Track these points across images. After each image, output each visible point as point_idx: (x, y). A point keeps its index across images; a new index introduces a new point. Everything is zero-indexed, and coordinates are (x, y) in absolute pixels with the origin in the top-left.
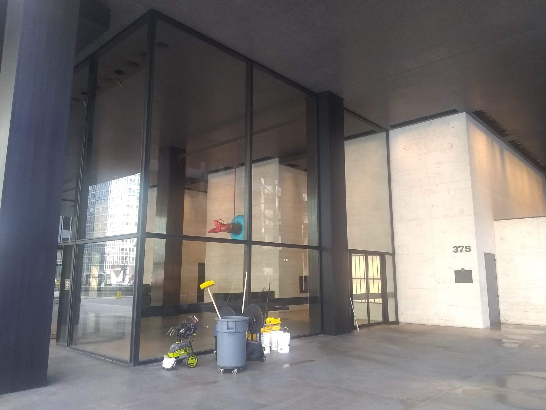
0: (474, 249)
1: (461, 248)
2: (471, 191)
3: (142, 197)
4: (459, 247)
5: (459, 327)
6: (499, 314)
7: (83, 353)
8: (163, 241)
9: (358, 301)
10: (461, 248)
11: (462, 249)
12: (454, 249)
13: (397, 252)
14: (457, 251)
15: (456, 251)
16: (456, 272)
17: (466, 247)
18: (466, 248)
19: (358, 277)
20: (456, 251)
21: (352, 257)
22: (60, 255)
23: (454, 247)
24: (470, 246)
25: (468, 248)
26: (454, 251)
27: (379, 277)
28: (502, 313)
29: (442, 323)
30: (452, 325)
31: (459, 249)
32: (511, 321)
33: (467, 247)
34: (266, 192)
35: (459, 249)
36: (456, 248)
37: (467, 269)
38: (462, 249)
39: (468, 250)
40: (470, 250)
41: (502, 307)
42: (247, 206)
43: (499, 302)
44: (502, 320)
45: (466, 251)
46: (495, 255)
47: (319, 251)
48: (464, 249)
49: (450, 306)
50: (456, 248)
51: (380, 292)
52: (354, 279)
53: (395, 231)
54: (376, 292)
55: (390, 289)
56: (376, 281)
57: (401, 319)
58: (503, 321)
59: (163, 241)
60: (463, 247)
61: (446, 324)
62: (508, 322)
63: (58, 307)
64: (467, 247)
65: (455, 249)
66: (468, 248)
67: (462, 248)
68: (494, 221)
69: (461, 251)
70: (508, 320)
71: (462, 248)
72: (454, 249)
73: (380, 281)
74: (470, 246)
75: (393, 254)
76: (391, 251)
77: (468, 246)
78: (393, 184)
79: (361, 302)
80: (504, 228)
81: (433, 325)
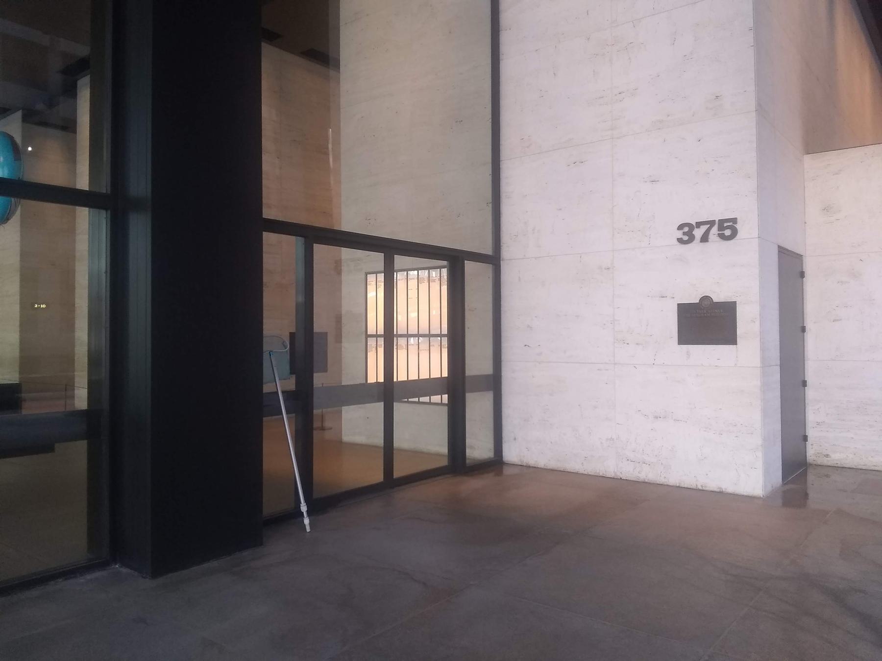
0: (748, 230)
1: (704, 228)
2: (752, 25)
4: (699, 224)
5: (682, 485)
6: (805, 438)
9: (422, 399)
10: (704, 228)
12: (679, 234)
13: (506, 253)
14: (692, 238)
15: (686, 238)
16: (685, 311)
17: (722, 222)
18: (721, 227)
19: (413, 330)
20: (686, 238)
23: (680, 227)
24: (734, 220)
25: (728, 227)
26: (680, 241)
27: (445, 331)
28: (812, 433)
29: (628, 471)
30: (661, 480)
31: (698, 233)
32: (838, 457)
35: (698, 233)
36: (686, 229)
37: (719, 296)
39: (728, 232)
40: (735, 233)
41: (812, 417)
43: (806, 402)
44: (812, 453)
45: (723, 237)
46: (804, 258)
47: (109, 212)
48: (715, 230)
49: (656, 417)
50: (686, 229)
51: (445, 374)
52: (402, 336)
53: (506, 188)
54: (436, 374)
56: (436, 341)
57: (511, 454)
58: (813, 458)
60: (712, 223)
61: (639, 475)
62: (825, 461)
63: (466, 372)
64: (725, 225)
65: (684, 234)
66: (728, 227)
67: (706, 227)
68: (805, 156)
69: (705, 239)
70: (827, 456)
71: (706, 227)
72: (681, 232)
73: (445, 341)
75: (494, 260)
76: (488, 250)
78: (506, 38)
79: (430, 403)
80: (837, 174)
81: (601, 474)
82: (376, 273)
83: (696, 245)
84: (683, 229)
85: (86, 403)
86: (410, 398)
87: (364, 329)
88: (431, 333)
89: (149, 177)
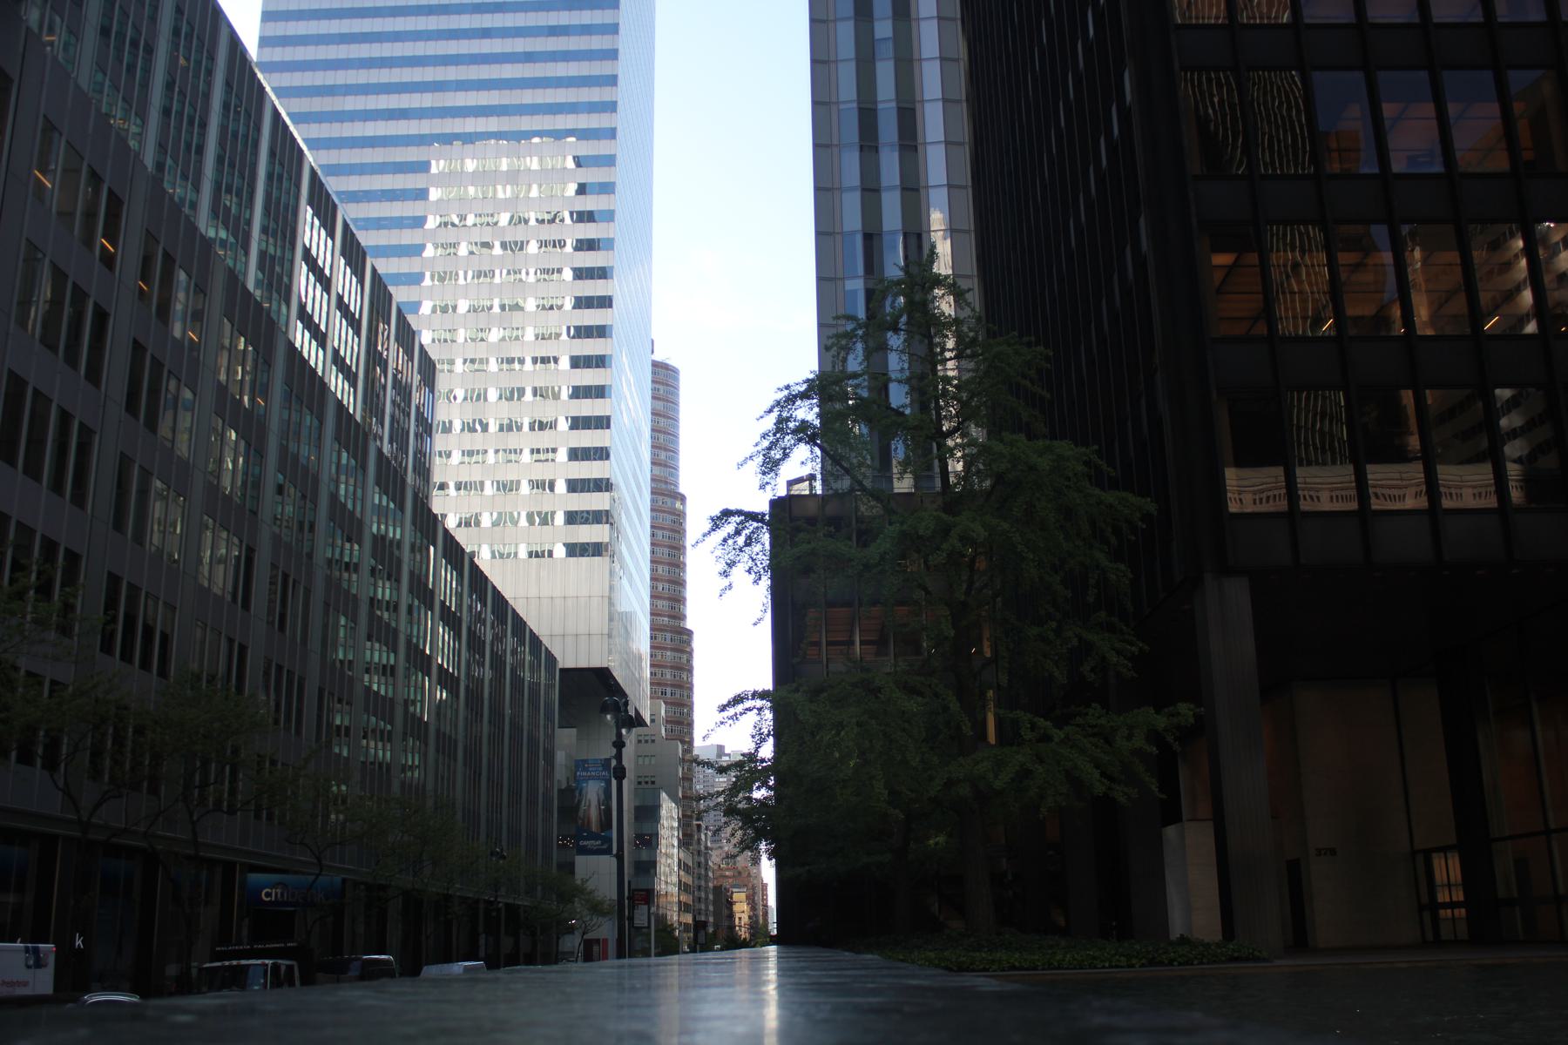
31: (1323, 852)
35: (1323, 852)
55: (1427, 916)
82: (1444, 850)
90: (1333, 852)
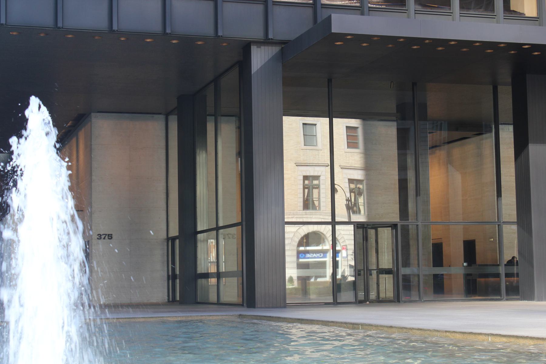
3: (366, 203)
4: (103, 235)
7: (168, 319)
8: (335, 120)
10: (104, 236)
11: (105, 237)
12: (98, 237)
15: (99, 238)
17: (108, 235)
20: (99, 238)
21: (516, 221)
22: (178, 299)
23: (98, 235)
24: (112, 235)
26: (98, 239)
31: (103, 237)
33: (110, 235)
34: (102, 303)
35: (103, 237)
36: (99, 236)
38: (105, 237)
42: (224, 306)
45: (109, 239)
48: (107, 237)
59: (335, 120)
60: (106, 235)
64: (110, 235)
65: (99, 237)
66: (110, 236)
67: (105, 235)
69: (104, 238)
71: (105, 235)
72: (98, 236)
74: (112, 235)
77: (110, 234)
78: (165, 191)
83: (102, 240)
84: (93, 321)
85: (500, 127)
86: (492, 52)
87: (307, 145)
88: (327, 120)
89: (408, 162)
90: (110, 237)
